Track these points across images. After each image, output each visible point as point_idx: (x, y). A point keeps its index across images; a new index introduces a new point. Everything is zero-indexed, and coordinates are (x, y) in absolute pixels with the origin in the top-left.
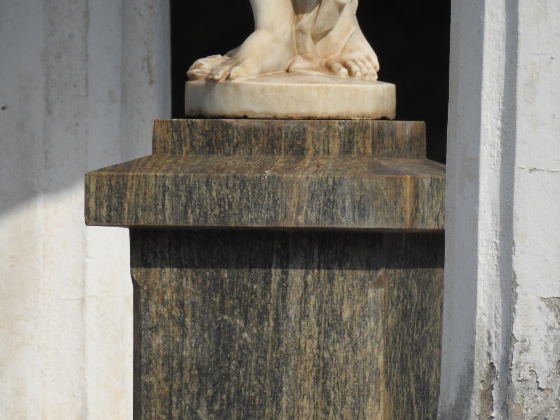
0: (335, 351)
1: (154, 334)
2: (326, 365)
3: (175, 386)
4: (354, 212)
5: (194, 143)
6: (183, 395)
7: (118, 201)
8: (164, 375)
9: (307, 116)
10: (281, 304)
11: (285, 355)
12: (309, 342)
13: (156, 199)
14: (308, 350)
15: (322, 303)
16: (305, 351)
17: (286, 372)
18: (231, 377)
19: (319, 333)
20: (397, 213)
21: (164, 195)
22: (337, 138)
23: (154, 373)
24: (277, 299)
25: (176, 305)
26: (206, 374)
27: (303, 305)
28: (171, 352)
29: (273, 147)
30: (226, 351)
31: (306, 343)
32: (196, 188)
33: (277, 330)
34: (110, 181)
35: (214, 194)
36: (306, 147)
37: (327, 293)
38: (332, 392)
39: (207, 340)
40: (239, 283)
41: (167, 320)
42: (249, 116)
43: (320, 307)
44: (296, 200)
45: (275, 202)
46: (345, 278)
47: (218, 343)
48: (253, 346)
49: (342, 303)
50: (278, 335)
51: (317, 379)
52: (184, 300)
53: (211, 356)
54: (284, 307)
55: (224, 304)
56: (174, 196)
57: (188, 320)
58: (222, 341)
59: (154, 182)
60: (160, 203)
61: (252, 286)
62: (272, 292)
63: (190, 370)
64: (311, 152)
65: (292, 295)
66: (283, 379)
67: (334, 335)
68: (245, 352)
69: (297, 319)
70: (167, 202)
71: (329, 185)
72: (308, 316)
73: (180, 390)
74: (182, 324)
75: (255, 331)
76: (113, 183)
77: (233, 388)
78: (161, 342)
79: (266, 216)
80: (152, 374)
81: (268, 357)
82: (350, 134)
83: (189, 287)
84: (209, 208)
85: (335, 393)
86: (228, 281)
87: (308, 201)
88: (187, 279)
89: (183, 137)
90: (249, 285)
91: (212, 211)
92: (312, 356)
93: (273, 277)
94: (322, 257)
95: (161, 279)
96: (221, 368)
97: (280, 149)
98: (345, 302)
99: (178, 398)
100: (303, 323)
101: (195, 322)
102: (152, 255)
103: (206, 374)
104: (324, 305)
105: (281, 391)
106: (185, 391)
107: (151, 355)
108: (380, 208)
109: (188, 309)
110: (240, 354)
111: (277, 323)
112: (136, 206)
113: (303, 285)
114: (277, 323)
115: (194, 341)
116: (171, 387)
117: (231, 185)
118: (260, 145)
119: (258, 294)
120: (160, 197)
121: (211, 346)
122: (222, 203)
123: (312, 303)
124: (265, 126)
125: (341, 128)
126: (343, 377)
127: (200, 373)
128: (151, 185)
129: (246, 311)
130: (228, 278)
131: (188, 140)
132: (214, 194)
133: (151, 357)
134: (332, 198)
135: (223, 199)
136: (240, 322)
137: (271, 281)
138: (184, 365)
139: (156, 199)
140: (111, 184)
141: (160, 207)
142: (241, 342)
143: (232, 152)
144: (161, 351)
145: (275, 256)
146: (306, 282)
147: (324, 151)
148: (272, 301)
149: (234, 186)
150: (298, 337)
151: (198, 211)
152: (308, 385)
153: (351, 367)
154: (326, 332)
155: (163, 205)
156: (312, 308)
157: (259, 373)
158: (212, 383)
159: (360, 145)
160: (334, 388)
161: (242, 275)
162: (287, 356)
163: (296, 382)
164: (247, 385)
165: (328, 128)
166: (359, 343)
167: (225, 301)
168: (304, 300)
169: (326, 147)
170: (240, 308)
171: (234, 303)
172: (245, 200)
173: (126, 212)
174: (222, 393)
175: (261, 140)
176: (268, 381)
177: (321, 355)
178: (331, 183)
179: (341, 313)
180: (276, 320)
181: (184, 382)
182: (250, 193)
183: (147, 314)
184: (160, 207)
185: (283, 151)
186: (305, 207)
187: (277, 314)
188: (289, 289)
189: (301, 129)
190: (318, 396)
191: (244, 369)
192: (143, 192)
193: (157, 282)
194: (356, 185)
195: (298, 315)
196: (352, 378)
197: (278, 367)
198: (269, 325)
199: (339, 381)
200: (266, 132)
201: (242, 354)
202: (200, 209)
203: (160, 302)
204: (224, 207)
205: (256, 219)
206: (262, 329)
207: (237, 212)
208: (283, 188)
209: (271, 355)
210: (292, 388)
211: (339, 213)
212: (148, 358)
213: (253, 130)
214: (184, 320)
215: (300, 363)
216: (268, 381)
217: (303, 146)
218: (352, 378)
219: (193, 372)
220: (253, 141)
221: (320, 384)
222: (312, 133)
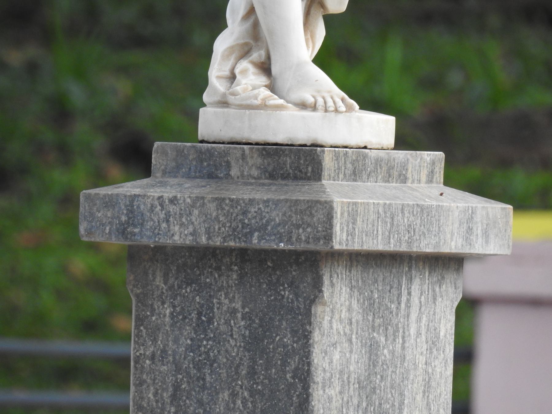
0: (435, 366)
1: (334, 350)
2: (430, 378)
3: (345, 399)
4: (482, 239)
5: (346, 172)
6: (349, 407)
7: (352, 226)
8: (339, 388)
9: (335, 146)
10: (406, 323)
11: (407, 370)
12: (421, 357)
13: (373, 226)
14: (420, 366)
15: (429, 322)
16: (418, 366)
17: (407, 386)
18: (376, 390)
19: (427, 350)
20: (506, 240)
21: (378, 221)
22: (425, 168)
23: (333, 387)
24: (404, 318)
25: (348, 323)
26: (363, 387)
27: (418, 324)
28: (344, 366)
29: (390, 176)
30: (374, 366)
31: (419, 359)
32: (395, 215)
33: (403, 348)
34: (349, 207)
35: (406, 220)
36: (408, 177)
37: (432, 313)
38: (432, 405)
39: (364, 356)
40: (383, 303)
41: (342, 337)
42: (369, 147)
43: (428, 325)
44: (451, 227)
45: (439, 230)
46: (443, 299)
47: (370, 359)
48: (389, 362)
49: (440, 323)
50: (404, 352)
51: (424, 392)
52: (352, 318)
53: (366, 370)
54: (408, 325)
55: (374, 323)
56: (383, 222)
57: (354, 337)
58: (372, 357)
59: (373, 210)
60: (375, 230)
61: (391, 306)
62: (402, 311)
63: (354, 384)
64: (410, 181)
65: (413, 315)
66: (406, 392)
67: (435, 352)
68: (385, 367)
69: (415, 337)
70: (380, 227)
71: (469, 214)
72: (421, 334)
73: (348, 403)
74: (350, 341)
75: (391, 348)
76: (350, 209)
77: (377, 400)
78: (338, 357)
79: (434, 241)
80: (332, 388)
81: (397, 372)
82: (433, 165)
83: (355, 306)
84: (402, 234)
85: (434, 405)
86: (377, 300)
87: (458, 228)
88: (354, 299)
89: (340, 165)
90: (389, 304)
91: (404, 237)
92: (422, 371)
93: (403, 297)
94: (430, 279)
95: (340, 299)
96: (371, 382)
97: (393, 177)
98: (442, 321)
99: (346, 409)
100: (418, 340)
101: (358, 339)
102: (336, 276)
103: (363, 387)
104: (430, 324)
105: (404, 403)
106: (350, 404)
107: (332, 369)
108: (497, 235)
109: (354, 326)
110: (382, 369)
111: (404, 342)
112: (363, 232)
113: (419, 305)
114: (404, 342)
115: (356, 356)
116: (343, 399)
117: (415, 213)
118: (382, 174)
119: (394, 313)
120: (376, 222)
121: (366, 361)
122: (410, 229)
123: (424, 322)
124: (386, 157)
125: (428, 159)
126: (439, 391)
127: (359, 387)
128: (371, 211)
129: (387, 329)
130: (377, 298)
131: (343, 168)
132: (406, 220)
133: (332, 372)
134: (471, 225)
135: (410, 225)
136: (383, 339)
137: (401, 301)
138: (350, 379)
139: (373, 226)
140: (349, 210)
141: (375, 232)
142: (383, 358)
143: (366, 180)
144: (338, 366)
145: (404, 279)
146: (420, 302)
147: (417, 180)
148: (401, 320)
149: (417, 214)
150: (415, 353)
151: (396, 236)
152: (419, 397)
153: (443, 381)
154: (431, 349)
155: (377, 231)
156: (423, 327)
157: (392, 387)
158: (366, 396)
159: (438, 175)
160: (433, 401)
161: (385, 296)
162: (408, 371)
163: (412, 395)
164: (385, 398)
165: (421, 159)
166: (448, 360)
167: (375, 319)
168: (419, 320)
169: (419, 176)
170: (383, 326)
171: (380, 321)
172: (422, 227)
173: (357, 236)
174: (371, 406)
175: (383, 169)
176: (397, 395)
177: (427, 370)
178: (470, 212)
179: (440, 331)
180: (403, 337)
181: (350, 394)
182: (426, 220)
183: (331, 331)
184: (375, 232)
185: (395, 180)
186: (456, 234)
187: (404, 332)
188: (411, 308)
189: (406, 160)
190: (424, 408)
191: (384, 383)
192: (367, 218)
193: (338, 301)
194: (484, 214)
195: (416, 333)
196: (444, 391)
197: (403, 381)
198: (399, 343)
199: (437, 395)
200: (386, 162)
201: (383, 369)
202: (397, 234)
203: (339, 320)
204: (411, 233)
205: (428, 244)
206: (395, 346)
207: (418, 238)
208: (444, 216)
209: (400, 370)
210: (410, 400)
211: (474, 239)
212: (330, 372)
213: (379, 160)
214: (352, 337)
215: (415, 377)
216: (397, 395)
217: (406, 175)
218: (444, 391)
219: (355, 386)
220: (379, 171)
221: (426, 397)
222: (412, 162)
